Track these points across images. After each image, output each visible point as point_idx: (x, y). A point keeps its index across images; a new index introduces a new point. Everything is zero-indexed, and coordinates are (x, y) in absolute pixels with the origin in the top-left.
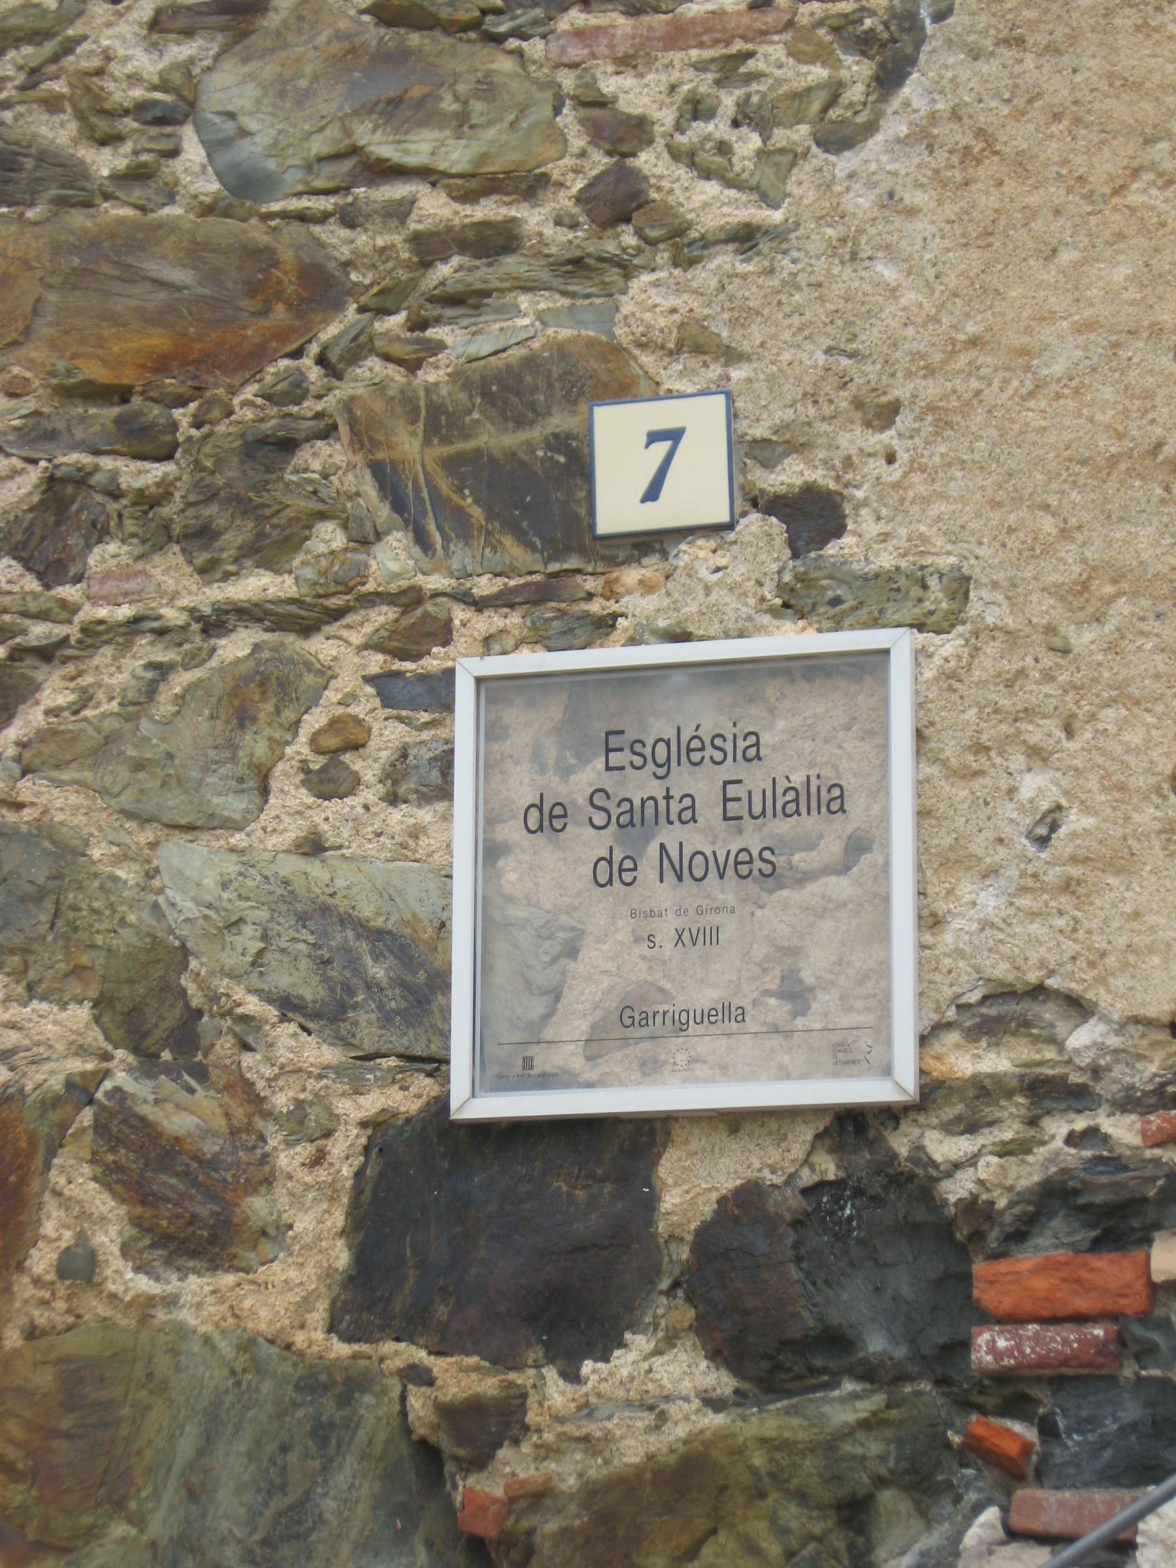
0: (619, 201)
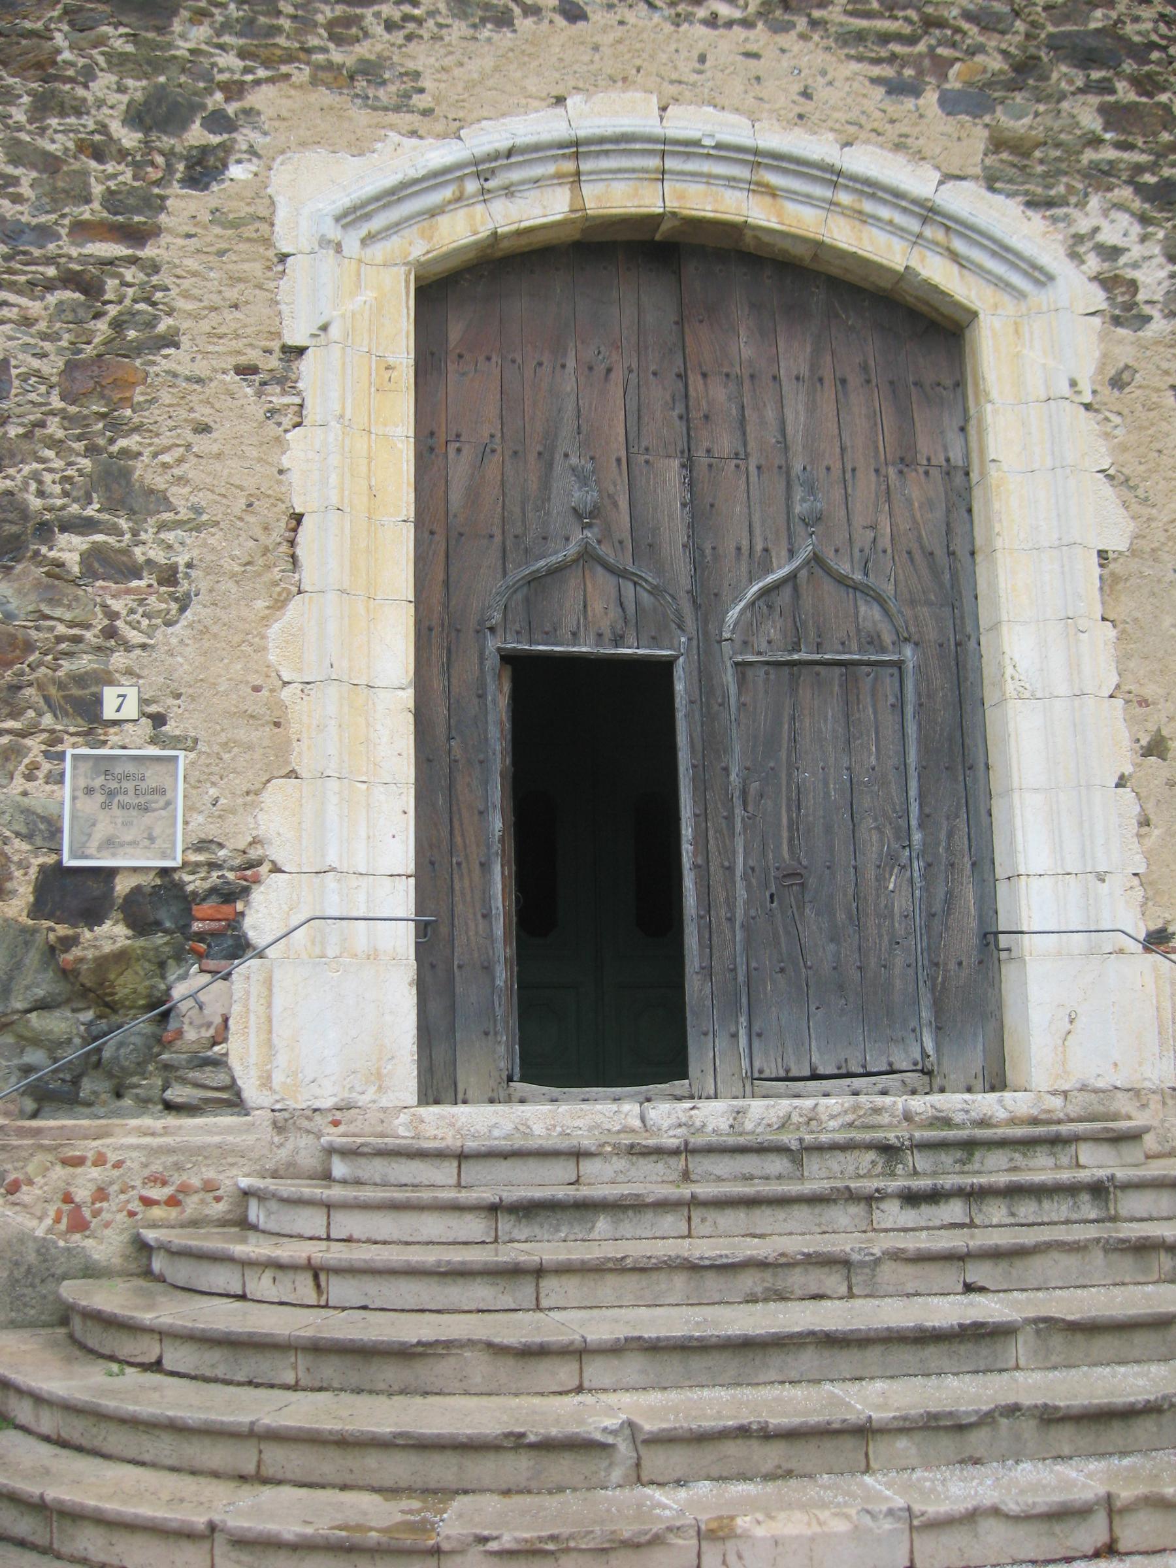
0: (110, 633)
